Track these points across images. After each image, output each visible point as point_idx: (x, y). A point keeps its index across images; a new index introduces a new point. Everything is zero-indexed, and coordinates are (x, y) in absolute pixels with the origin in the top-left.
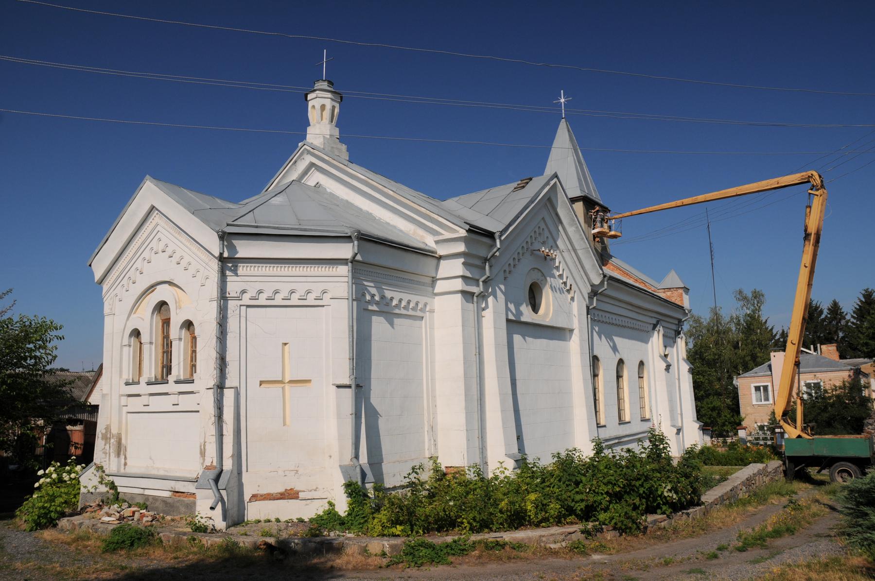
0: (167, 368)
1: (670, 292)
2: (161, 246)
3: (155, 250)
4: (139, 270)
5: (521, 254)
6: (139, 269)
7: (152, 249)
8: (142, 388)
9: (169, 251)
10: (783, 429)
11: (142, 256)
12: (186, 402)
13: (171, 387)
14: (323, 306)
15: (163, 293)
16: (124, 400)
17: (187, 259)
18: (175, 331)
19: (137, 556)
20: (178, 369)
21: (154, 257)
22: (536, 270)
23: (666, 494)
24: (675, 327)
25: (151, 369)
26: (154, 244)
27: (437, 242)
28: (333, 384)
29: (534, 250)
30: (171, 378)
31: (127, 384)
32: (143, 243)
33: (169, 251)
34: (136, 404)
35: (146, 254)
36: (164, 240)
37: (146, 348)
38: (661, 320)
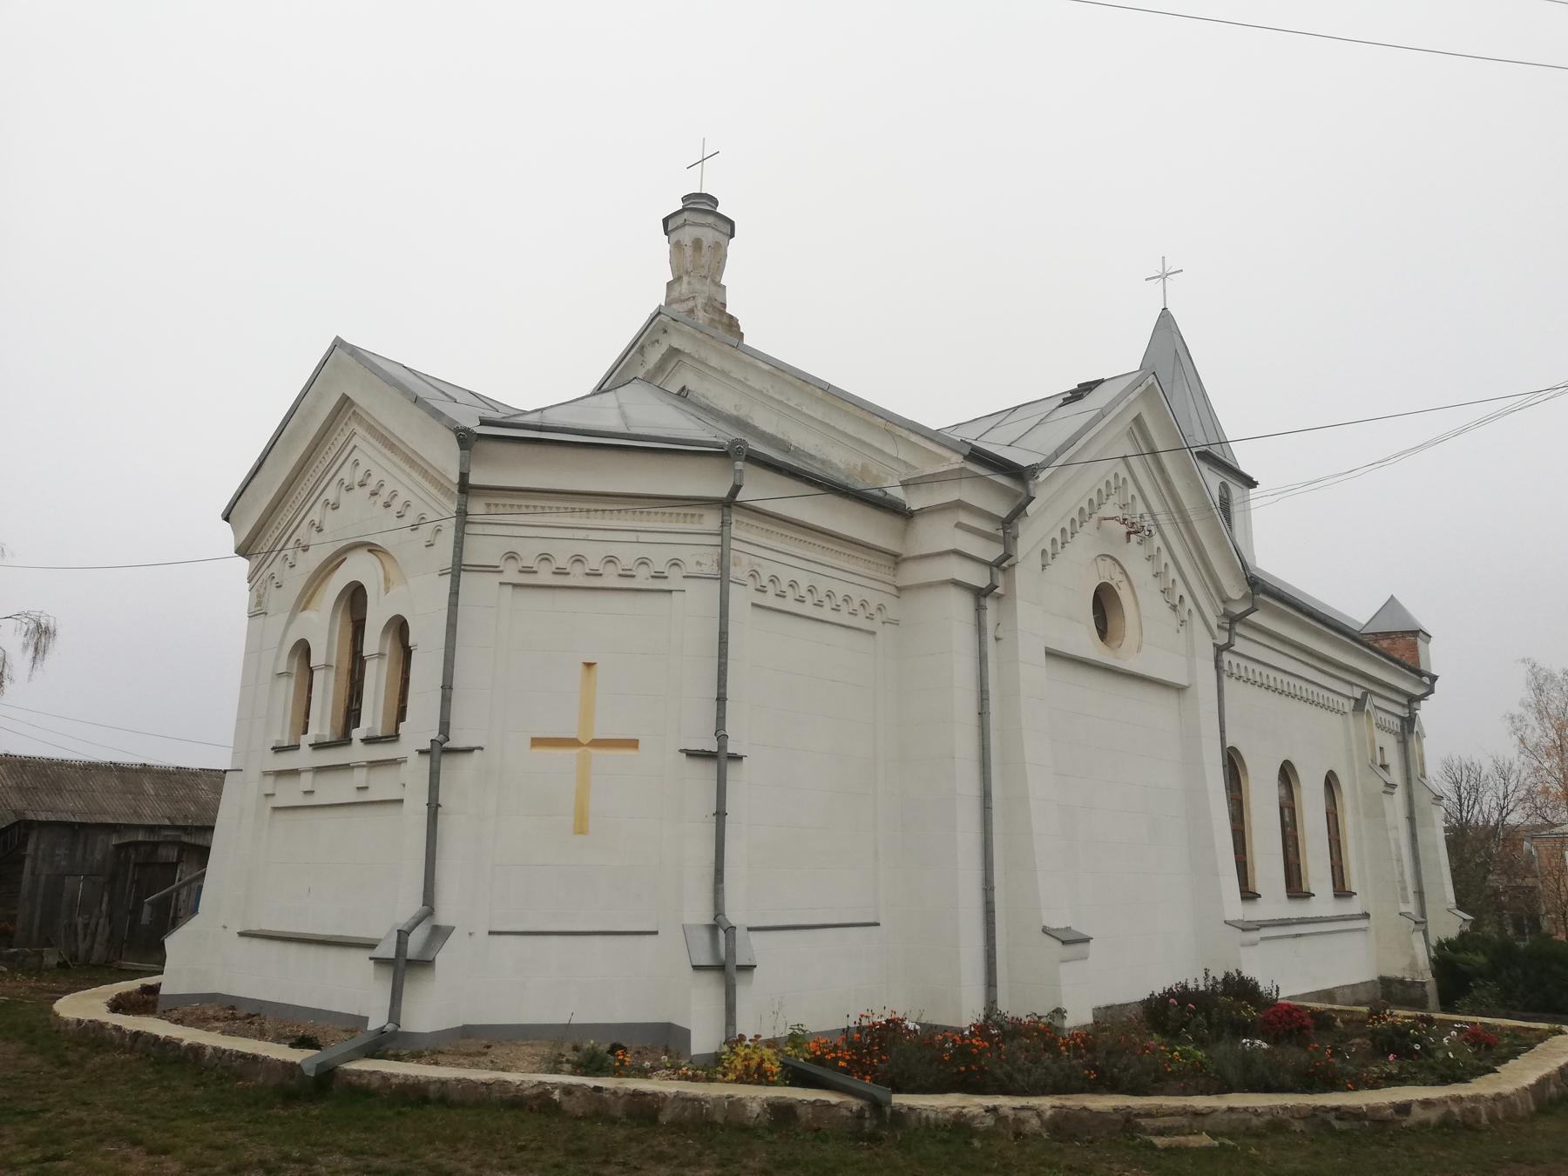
0: (352, 716)
1: (1389, 641)
2: (359, 476)
3: (346, 483)
4: (317, 524)
5: (1078, 524)
6: (317, 524)
7: (341, 481)
8: (305, 758)
9: (372, 484)
10: (731, 1081)
11: (322, 499)
12: (383, 785)
13: (357, 752)
14: (671, 591)
15: (359, 568)
16: (269, 785)
17: (403, 495)
18: (373, 640)
19: (89, 923)
20: (372, 718)
21: (345, 498)
22: (1108, 559)
23: (440, 1124)
24: (1404, 713)
25: (322, 724)
26: (345, 474)
27: (905, 485)
28: (681, 751)
29: (1105, 519)
30: (357, 734)
31: (278, 750)
32: (326, 472)
33: (372, 484)
34: (289, 793)
35: (330, 495)
36: (365, 464)
37: (318, 677)
38: (1372, 693)
